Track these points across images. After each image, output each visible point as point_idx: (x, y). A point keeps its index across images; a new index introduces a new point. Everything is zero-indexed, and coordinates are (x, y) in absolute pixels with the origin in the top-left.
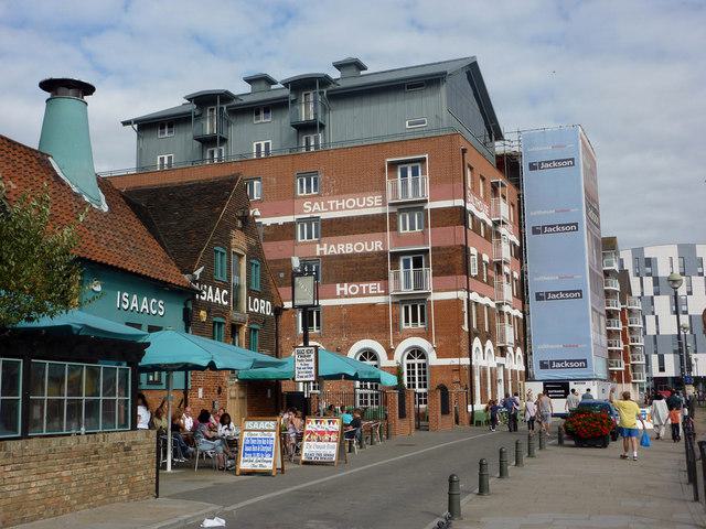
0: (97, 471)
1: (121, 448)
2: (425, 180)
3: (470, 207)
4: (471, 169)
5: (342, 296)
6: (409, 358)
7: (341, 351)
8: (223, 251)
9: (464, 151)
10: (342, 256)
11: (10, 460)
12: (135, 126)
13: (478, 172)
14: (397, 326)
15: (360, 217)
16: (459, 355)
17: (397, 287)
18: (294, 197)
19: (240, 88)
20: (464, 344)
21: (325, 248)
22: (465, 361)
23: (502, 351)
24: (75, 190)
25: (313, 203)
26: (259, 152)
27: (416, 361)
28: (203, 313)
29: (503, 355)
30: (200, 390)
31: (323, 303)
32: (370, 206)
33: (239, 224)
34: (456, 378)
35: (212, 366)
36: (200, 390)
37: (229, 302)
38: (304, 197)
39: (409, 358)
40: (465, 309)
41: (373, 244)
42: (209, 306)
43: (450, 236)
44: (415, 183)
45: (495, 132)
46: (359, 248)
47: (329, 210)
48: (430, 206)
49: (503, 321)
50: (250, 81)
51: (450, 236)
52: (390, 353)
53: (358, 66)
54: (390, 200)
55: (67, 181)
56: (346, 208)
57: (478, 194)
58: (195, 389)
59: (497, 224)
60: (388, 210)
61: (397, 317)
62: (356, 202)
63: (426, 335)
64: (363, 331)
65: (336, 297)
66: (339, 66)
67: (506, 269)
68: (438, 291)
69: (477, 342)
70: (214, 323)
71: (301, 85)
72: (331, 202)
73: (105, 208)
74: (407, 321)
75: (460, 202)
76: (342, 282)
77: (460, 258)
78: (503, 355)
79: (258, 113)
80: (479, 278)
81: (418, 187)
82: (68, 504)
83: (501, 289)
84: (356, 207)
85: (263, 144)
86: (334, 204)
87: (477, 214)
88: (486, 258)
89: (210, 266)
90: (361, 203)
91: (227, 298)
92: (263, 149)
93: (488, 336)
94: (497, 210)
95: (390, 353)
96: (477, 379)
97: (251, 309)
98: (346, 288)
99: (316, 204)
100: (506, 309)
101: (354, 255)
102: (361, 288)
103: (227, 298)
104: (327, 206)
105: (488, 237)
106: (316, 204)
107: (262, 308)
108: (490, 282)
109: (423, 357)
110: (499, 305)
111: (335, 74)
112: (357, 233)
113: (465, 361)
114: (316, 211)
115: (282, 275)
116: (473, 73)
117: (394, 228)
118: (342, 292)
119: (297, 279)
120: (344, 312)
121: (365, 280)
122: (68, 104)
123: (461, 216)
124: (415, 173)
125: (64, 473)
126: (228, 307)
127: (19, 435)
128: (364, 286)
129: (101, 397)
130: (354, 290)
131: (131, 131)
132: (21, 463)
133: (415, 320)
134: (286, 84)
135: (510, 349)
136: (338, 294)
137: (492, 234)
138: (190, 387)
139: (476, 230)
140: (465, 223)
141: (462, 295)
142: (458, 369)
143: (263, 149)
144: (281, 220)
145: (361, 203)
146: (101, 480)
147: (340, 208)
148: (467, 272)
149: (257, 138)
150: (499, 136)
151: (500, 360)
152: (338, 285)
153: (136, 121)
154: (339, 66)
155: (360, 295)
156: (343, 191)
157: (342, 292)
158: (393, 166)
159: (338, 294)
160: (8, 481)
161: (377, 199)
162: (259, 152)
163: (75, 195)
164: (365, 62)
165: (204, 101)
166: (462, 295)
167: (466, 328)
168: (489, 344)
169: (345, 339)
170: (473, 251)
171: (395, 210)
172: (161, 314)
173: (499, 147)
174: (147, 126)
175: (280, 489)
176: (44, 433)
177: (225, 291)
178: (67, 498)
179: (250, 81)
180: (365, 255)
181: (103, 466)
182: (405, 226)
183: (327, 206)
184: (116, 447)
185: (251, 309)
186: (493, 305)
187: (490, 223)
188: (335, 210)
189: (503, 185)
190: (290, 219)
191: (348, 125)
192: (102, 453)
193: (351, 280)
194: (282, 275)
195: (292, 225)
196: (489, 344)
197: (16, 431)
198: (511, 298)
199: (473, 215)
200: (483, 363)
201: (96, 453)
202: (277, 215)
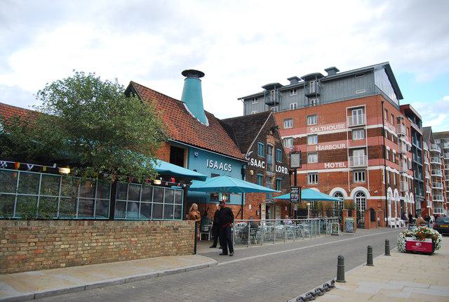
0: (155, 239)
2: (364, 116)
3: (385, 128)
4: (387, 111)
5: (327, 168)
6: (357, 196)
7: (327, 193)
9: (382, 102)
11: (96, 231)
13: (390, 112)
14: (351, 182)
16: (380, 194)
17: (352, 164)
18: (306, 126)
19: (286, 83)
20: (383, 190)
22: (384, 198)
23: (403, 194)
26: (292, 107)
27: (361, 197)
28: (252, 172)
29: (403, 196)
30: (250, 206)
32: (340, 128)
33: (271, 132)
34: (379, 205)
36: (250, 206)
39: (357, 196)
40: (384, 174)
41: (341, 145)
42: (255, 168)
43: (377, 141)
44: (360, 118)
45: (399, 96)
46: (335, 147)
48: (366, 128)
49: (402, 180)
50: (289, 79)
51: (377, 141)
52: (349, 194)
53: (335, 70)
54: (348, 126)
57: (390, 122)
58: (247, 205)
59: (400, 136)
60: (347, 130)
61: (351, 178)
62: (333, 127)
63: (365, 186)
64: (340, 184)
66: (327, 70)
67: (405, 157)
69: (389, 189)
70: (258, 176)
71: (309, 78)
73: (207, 124)
74: (356, 179)
75: (381, 126)
77: (381, 151)
78: (403, 196)
79: (292, 92)
80: (390, 160)
81: (360, 118)
82: (135, 255)
83: (402, 166)
87: (390, 131)
88: (394, 151)
89: (255, 148)
93: (397, 186)
94: (400, 129)
95: (349, 194)
96: (390, 206)
98: (329, 165)
100: (404, 175)
101: (332, 150)
104: (321, 129)
105: (395, 142)
108: (396, 162)
109: (342, 196)
110: (401, 173)
111: (325, 74)
113: (384, 198)
116: (387, 68)
117: (350, 138)
120: (328, 175)
121: (338, 161)
122: (193, 80)
123: (382, 132)
124: (360, 113)
125: (133, 239)
126: (264, 169)
128: (337, 163)
129: (152, 203)
130: (332, 165)
131: (241, 103)
132: (103, 232)
133: (360, 179)
134: (303, 78)
135: (407, 193)
137: (397, 141)
139: (389, 138)
140: (384, 135)
141: (382, 167)
142: (380, 201)
144: (300, 136)
146: (159, 244)
147: (326, 130)
148: (385, 157)
149: (294, 101)
150: (402, 98)
151: (403, 198)
154: (327, 70)
155: (335, 168)
156: (328, 122)
158: (350, 110)
160: (93, 241)
161: (343, 125)
162: (292, 107)
164: (338, 68)
165: (269, 88)
166: (382, 167)
167: (384, 182)
168: (396, 190)
170: (388, 148)
171: (350, 130)
173: (402, 103)
174: (247, 100)
175: (244, 257)
176: (14, 217)
178: (134, 252)
179: (289, 79)
180: (337, 150)
181: (159, 237)
182: (357, 136)
183: (321, 129)
184: (167, 229)
186: (398, 173)
187: (396, 135)
189: (402, 118)
191: (332, 94)
192: (159, 230)
193: (331, 161)
196: (396, 190)
198: (407, 170)
199: (388, 132)
200: (393, 199)
201: (155, 230)
202: (299, 133)
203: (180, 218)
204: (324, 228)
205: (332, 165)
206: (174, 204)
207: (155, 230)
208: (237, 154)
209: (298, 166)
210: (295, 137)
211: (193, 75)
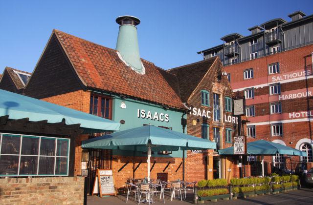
1: (48, 186)
5: (292, 118)
8: (207, 92)
10: (291, 100)
12: (203, 54)
15: (300, 81)
18: (268, 75)
21: (283, 97)
24: (127, 65)
25: (276, 77)
28: (195, 123)
31: (284, 122)
35: (294, 155)
37: (212, 116)
38: (272, 75)
46: (300, 95)
47: (285, 79)
55: (124, 61)
56: (293, 78)
62: (297, 74)
65: (289, 119)
68: (266, 87)
72: (285, 76)
76: (292, 112)
84: (298, 77)
85: (254, 54)
86: (287, 76)
90: (300, 74)
91: (209, 115)
92: (254, 56)
97: (226, 121)
98: (294, 115)
99: (278, 77)
101: (297, 99)
102: (301, 115)
103: (209, 115)
106: (278, 77)
107: (233, 120)
112: (298, 89)
114: (278, 80)
115: (264, 110)
118: (292, 116)
119: (235, 101)
120: (293, 126)
127: (68, 175)
128: (303, 113)
130: (298, 115)
136: (290, 117)
138: (186, 156)
143: (254, 56)
144: (262, 86)
145: (300, 74)
147: (290, 78)
152: (290, 113)
153: (202, 52)
155: (301, 117)
157: (292, 116)
159: (290, 117)
163: (127, 67)
169: (294, 138)
172: (167, 121)
177: (209, 112)
184: (40, 187)
185: (226, 121)
188: (287, 79)
190: (266, 85)
193: (296, 111)
194: (264, 110)
195: (268, 88)
197: (66, 174)
202: (261, 83)
203: (64, 172)
204: (199, 184)
205: (298, 115)
206: (56, 157)
207: (18, 189)
208: (177, 102)
209: (242, 113)
210: (256, 87)
211: (199, 53)
